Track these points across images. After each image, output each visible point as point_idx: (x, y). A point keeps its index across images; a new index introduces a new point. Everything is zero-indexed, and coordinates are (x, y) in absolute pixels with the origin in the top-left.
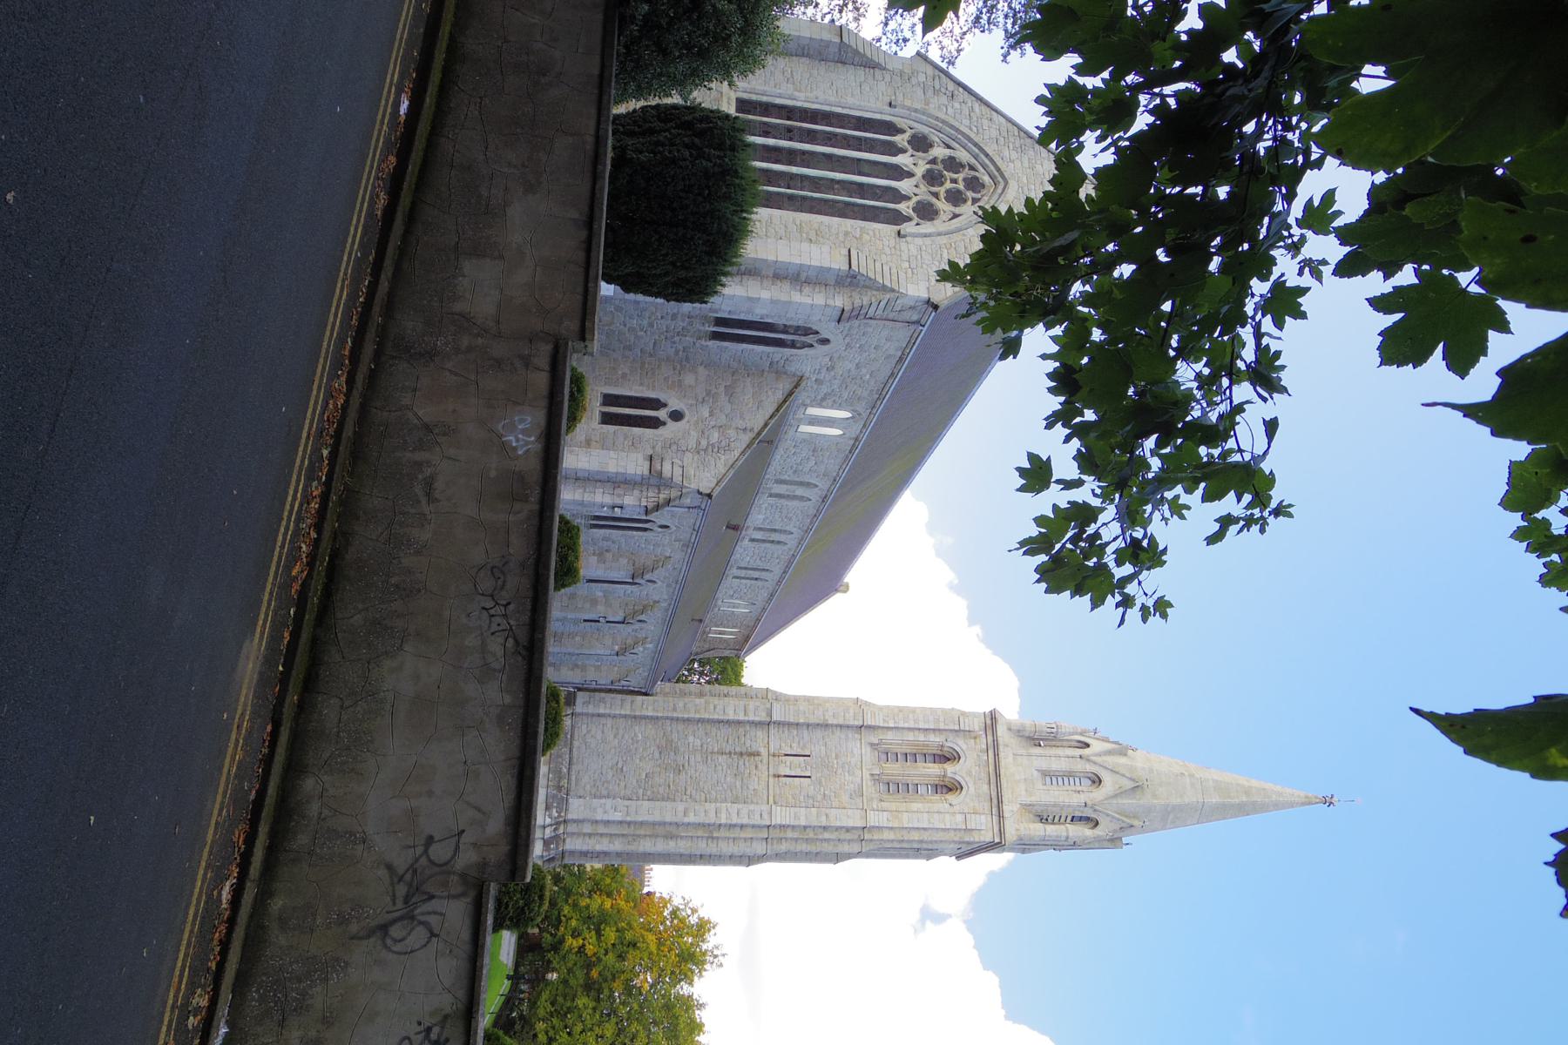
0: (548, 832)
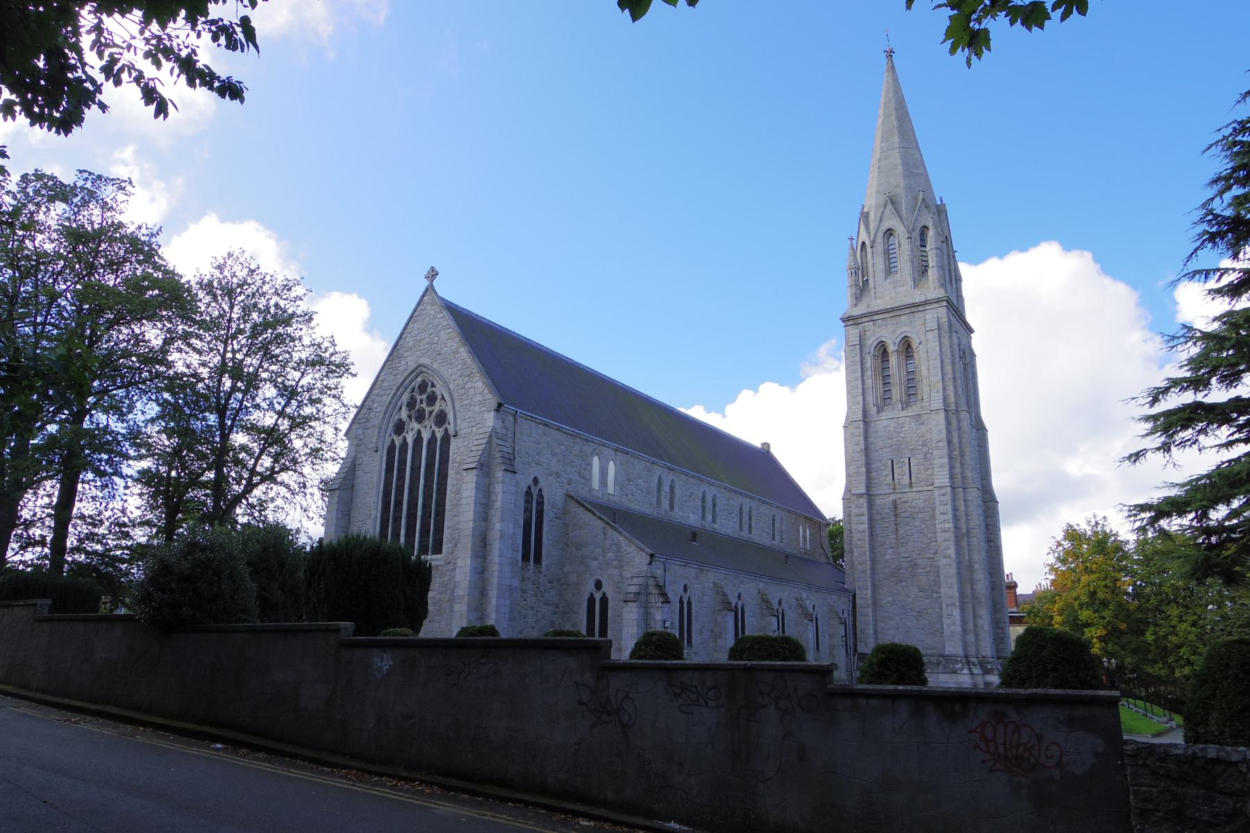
0: (976, 670)
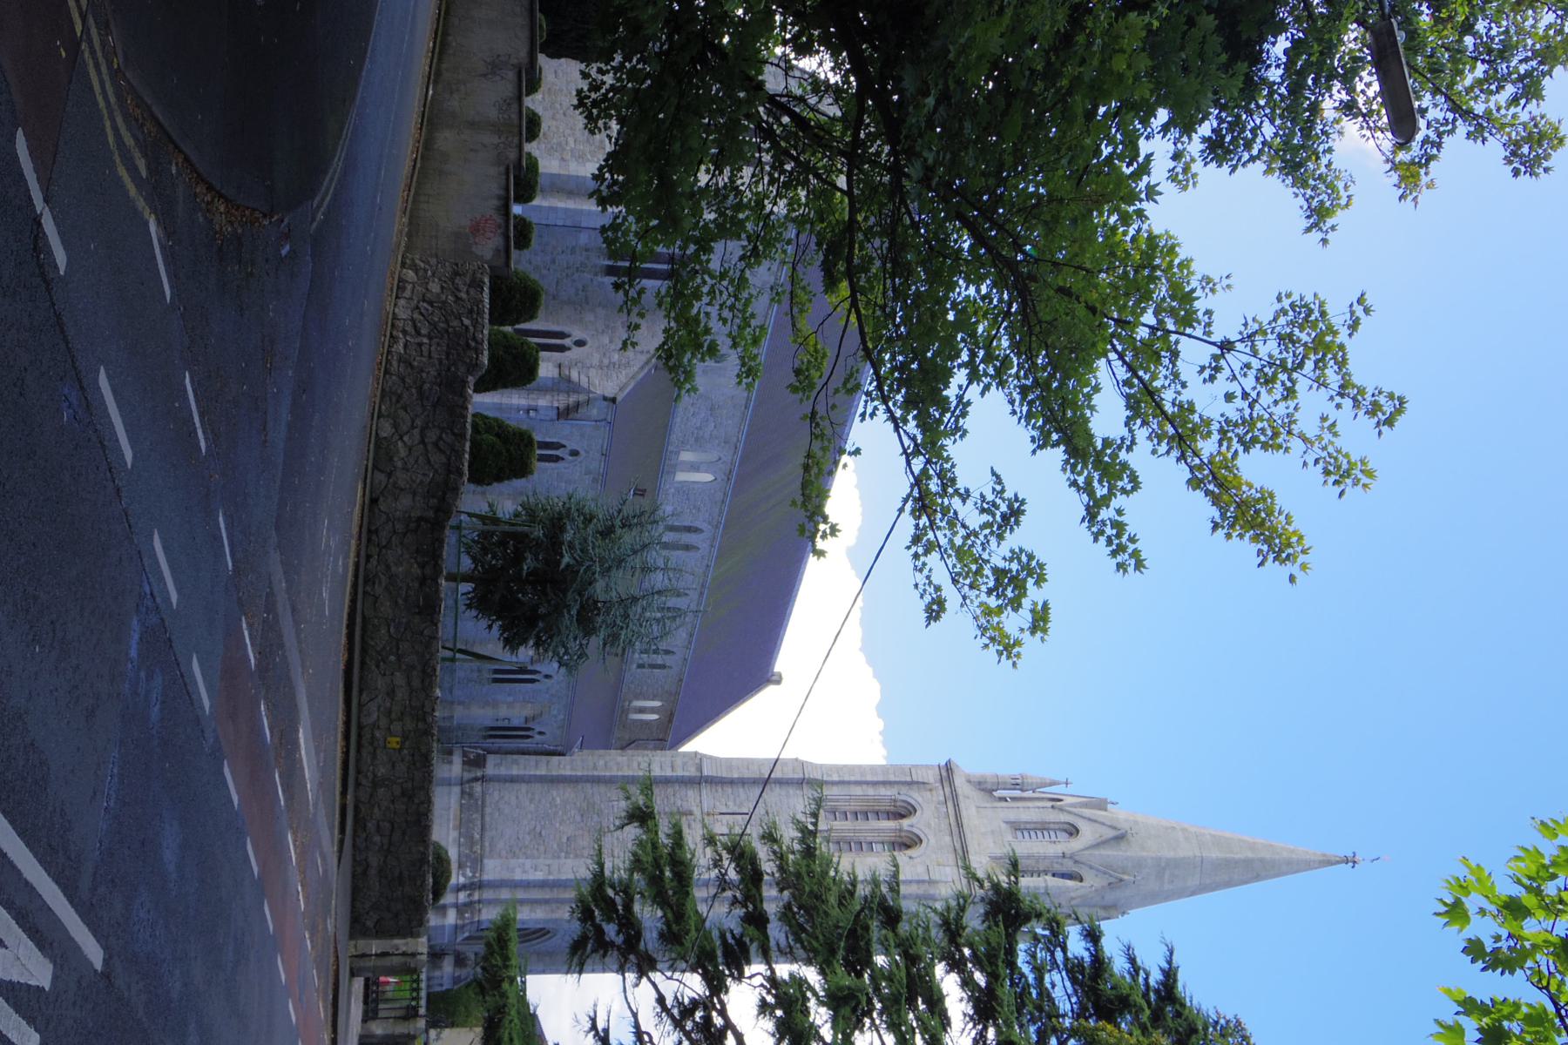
0: (462, 896)
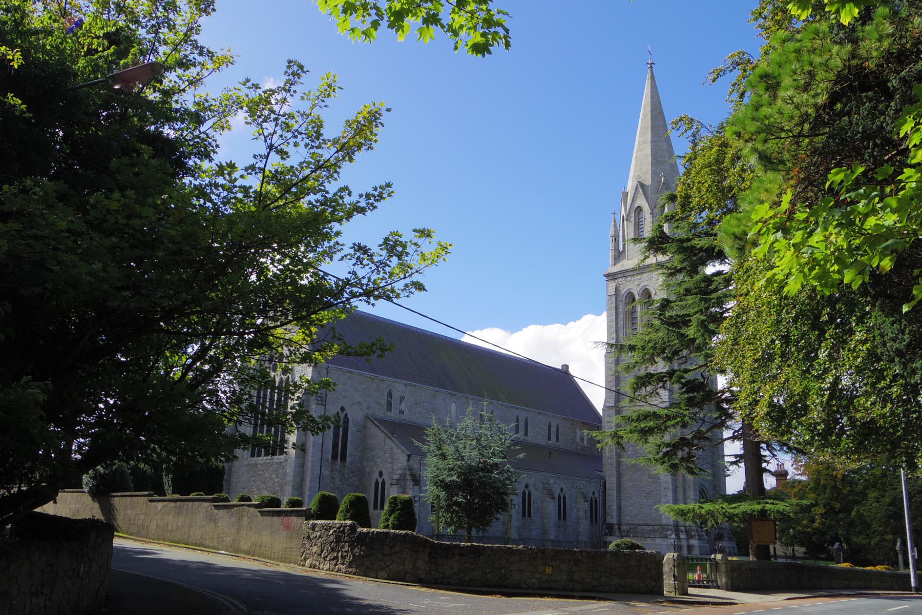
0: (683, 536)
